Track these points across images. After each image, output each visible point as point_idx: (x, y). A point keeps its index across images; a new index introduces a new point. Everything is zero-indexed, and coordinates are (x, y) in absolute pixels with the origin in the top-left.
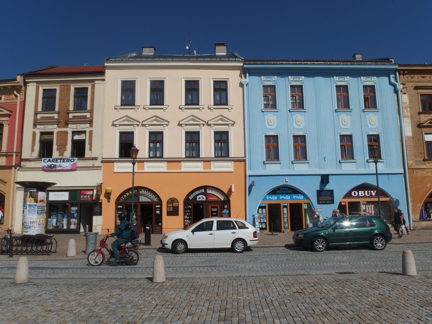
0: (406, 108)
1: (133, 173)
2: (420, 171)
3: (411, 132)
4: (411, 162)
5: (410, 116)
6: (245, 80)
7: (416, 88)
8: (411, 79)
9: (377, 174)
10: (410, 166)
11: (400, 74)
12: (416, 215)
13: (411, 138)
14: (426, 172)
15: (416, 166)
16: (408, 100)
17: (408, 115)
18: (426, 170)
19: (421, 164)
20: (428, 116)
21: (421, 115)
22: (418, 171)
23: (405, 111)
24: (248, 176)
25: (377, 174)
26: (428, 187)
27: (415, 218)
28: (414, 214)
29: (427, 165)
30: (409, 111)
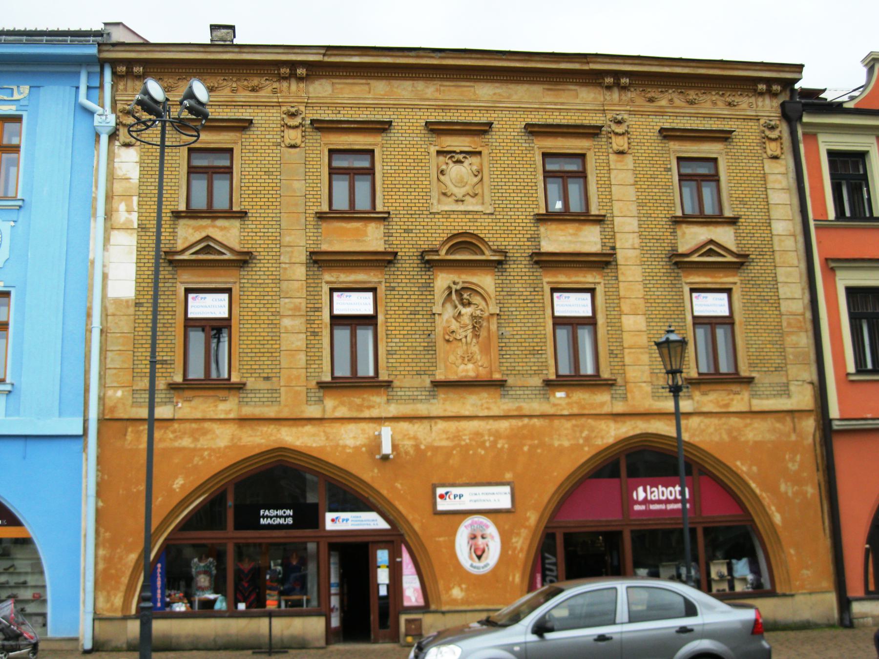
0: (127, 196)
1: (151, 421)
3: (133, 284)
4: (119, 393)
5: (136, 226)
7: (667, 134)
10: (113, 409)
11: (114, 73)
14: (174, 432)
15: (134, 410)
16: (138, 169)
17: (132, 221)
18: (176, 425)
20: (205, 227)
21: (182, 222)
23: (122, 207)
26: (174, 490)
27: (109, 605)
28: (108, 592)
29: (180, 405)
30: (136, 209)
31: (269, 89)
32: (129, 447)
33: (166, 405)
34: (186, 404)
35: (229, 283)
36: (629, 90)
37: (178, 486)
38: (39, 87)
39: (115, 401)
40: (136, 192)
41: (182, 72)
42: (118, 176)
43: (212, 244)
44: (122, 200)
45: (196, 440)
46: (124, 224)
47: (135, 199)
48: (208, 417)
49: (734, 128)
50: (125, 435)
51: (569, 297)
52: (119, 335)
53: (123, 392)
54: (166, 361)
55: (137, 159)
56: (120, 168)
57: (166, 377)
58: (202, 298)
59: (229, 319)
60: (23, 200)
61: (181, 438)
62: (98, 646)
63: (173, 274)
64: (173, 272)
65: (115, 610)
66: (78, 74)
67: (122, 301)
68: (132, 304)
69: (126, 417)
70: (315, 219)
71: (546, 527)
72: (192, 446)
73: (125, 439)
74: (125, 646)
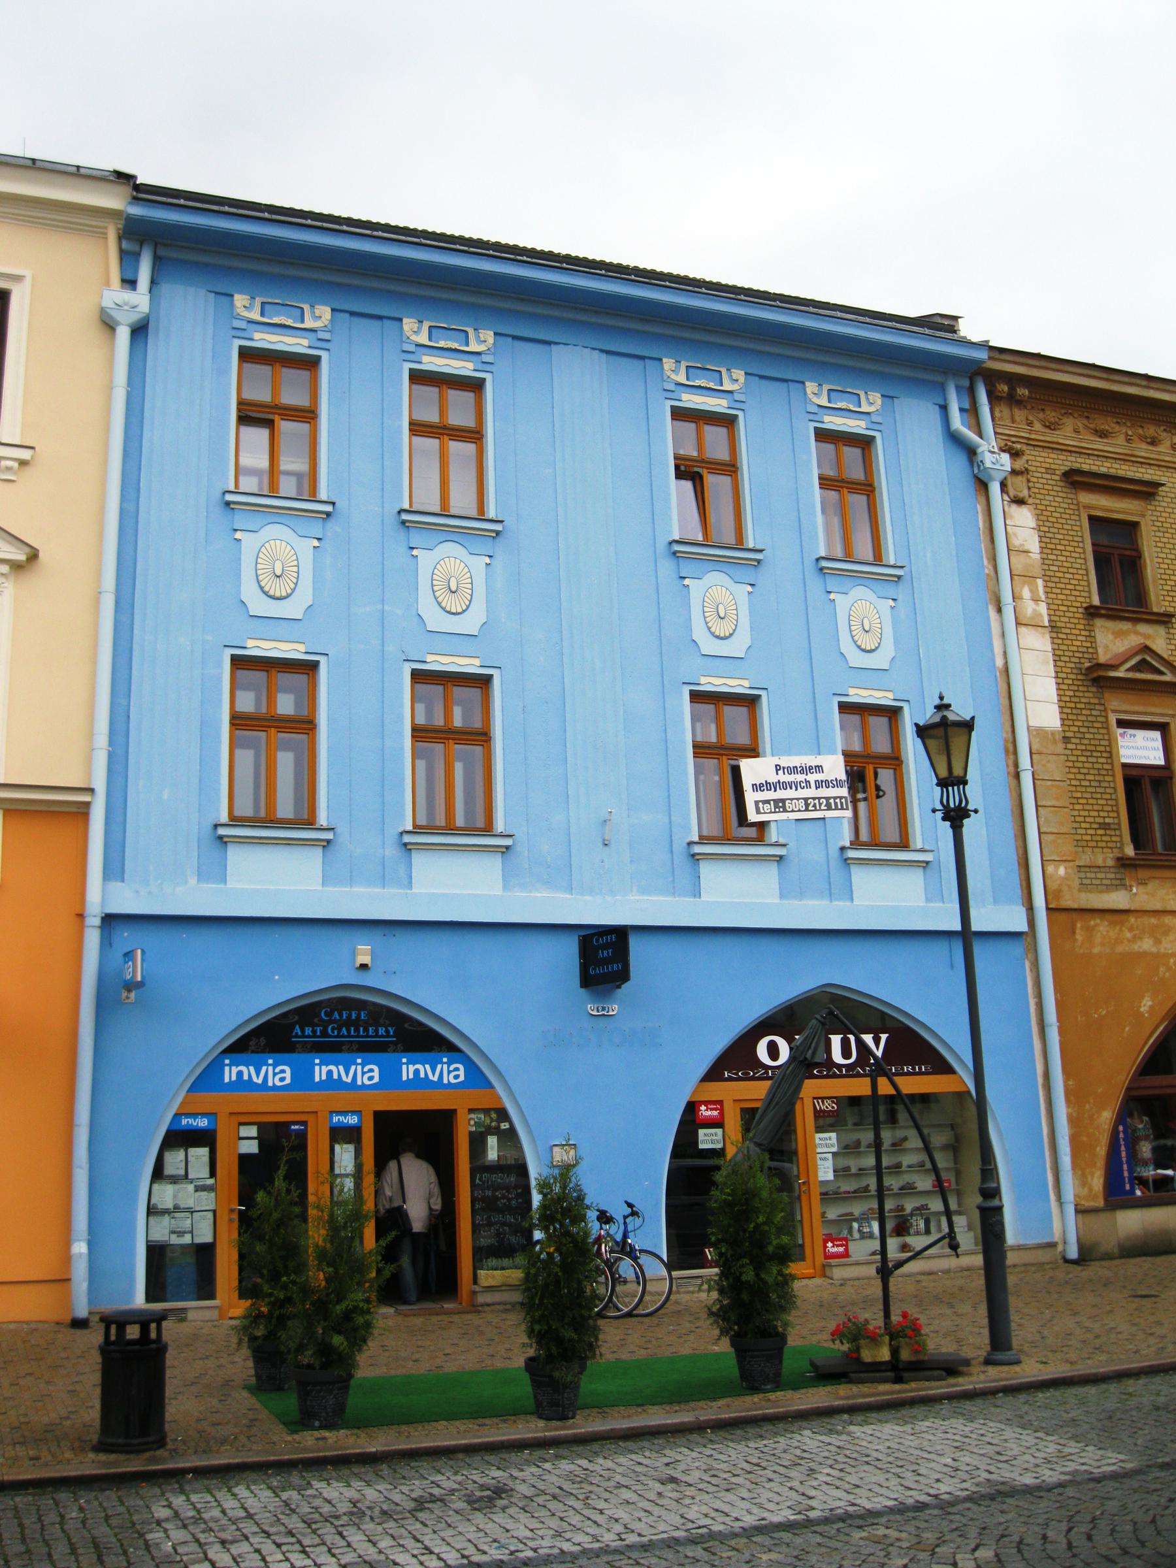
0: (1029, 578)
2: (1102, 927)
4: (1062, 871)
6: (127, 296)
8: (1047, 431)
9: (966, 936)
12: (1092, 1174)
13: (1055, 742)
14: (1131, 929)
19: (1110, 888)
21: (1099, 622)
22: (1092, 923)
24: (97, 921)
25: (966, 936)
26: (1142, 1014)
29: (1134, 890)
30: (1043, 597)
31: (1168, 443)
32: (1081, 951)
33: (1117, 890)
34: (1141, 889)
35: (1166, 715)
36: (1025, 407)
37: (1146, 1008)
38: (892, 397)
39: (1058, 882)
40: (1038, 571)
41: (1070, 405)
42: (1015, 547)
43: (1149, 659)
44: (1024, 583)
45: (1158, 942)
46: (1032, 618)
47: (1040, 582)
48: (1169, 908)
49: (1163, 480)
50: (1074, 932)
51: (1134, 736)
52: (1049, 783)
53: (1066, 868)
54: (1109, 824)
55: (1033, 525)
56: (1015, 535)
57: (1111, 848)
58: (1131, 735)
59: (1167, 767)
60: (334, 504)
61: (1141, 939)
62: (1087, 1255)
63: (1099, 698)
64: (1099, 695)
65: (1095, 1197)
66: (942, 387)
67: (1046, 732)
68: (1058, 737)
69: (1075, 906)
70: (1085, 617)
71: (1127, 1089)
72: (1154, 950)
73: (1075, 940)
74: (1116, 1250)
